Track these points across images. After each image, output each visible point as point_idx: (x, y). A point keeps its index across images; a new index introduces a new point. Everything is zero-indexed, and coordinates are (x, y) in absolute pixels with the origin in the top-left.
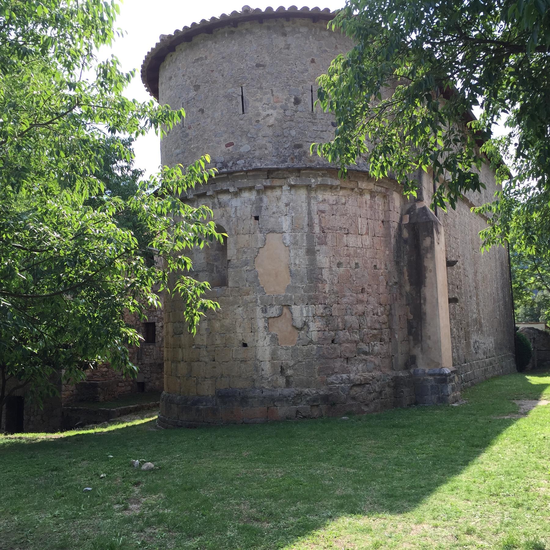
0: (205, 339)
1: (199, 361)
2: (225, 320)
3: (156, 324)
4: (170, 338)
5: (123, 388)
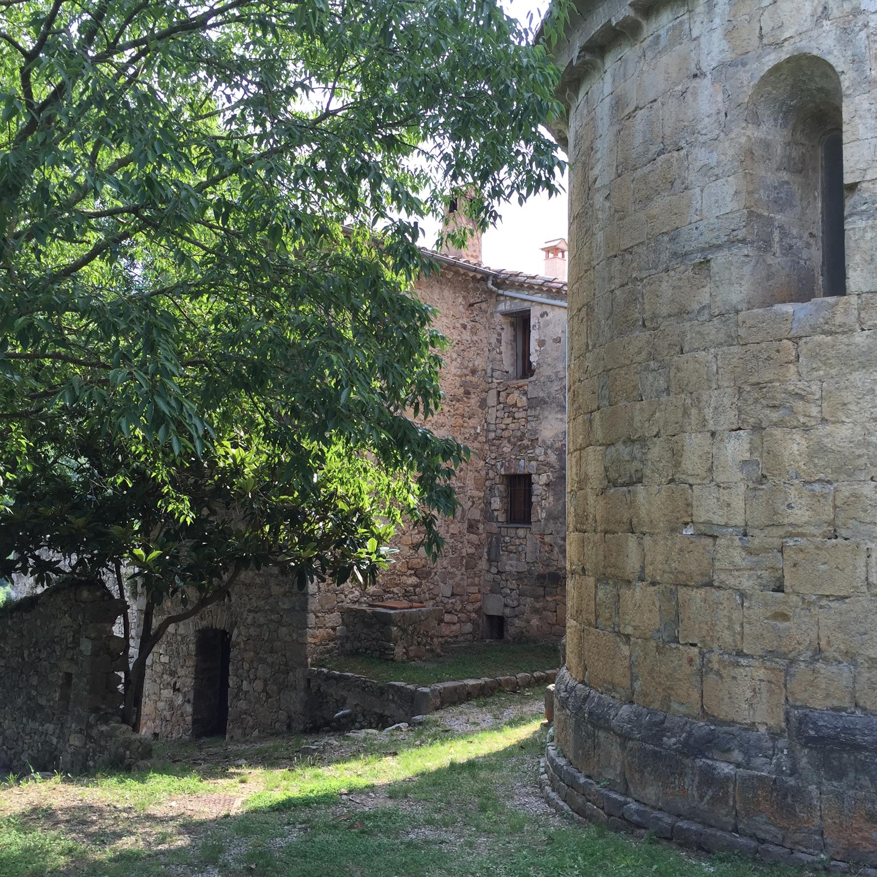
0: (738, 503)
1: (710, 584)
2: (829, 428)
3: (535, 477)
4: (591, 499)
5: (454, 628)
